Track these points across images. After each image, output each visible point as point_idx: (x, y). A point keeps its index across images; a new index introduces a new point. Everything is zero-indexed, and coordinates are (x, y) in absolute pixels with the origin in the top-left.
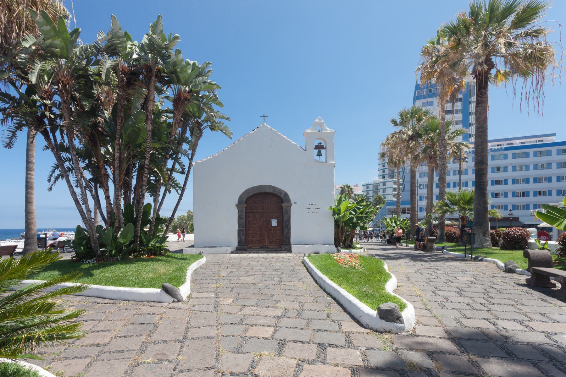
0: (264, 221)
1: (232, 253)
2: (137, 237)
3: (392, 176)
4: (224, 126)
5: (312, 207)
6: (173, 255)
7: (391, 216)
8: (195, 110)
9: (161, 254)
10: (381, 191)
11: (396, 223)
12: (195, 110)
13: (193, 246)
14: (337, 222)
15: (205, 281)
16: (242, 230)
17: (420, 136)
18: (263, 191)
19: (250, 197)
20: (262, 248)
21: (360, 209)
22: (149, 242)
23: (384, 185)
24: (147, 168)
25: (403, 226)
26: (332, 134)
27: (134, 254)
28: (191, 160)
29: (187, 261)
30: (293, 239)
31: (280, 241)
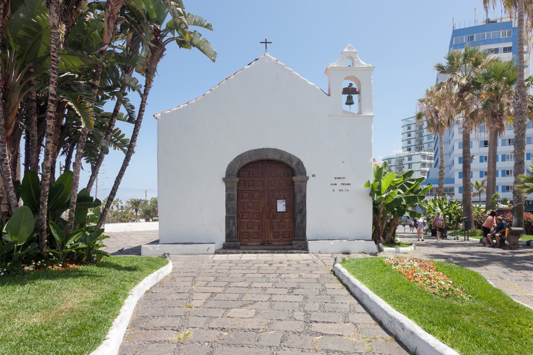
0: (265, 202)
1: (217, 252)
2: (42, 231)
3: (419, 148)
4: (201, 39)
5: (339, 182)
6: (114, 260)
7: (433, 197)
8: (152, 7)
9: (90, 261)
10: (406, 167)
11: (440, 206)
12: (152, 7)
13: (157, 242)
14: (375, 205)
15: (159, 322)
16: (233, 218)
17: (478, 86)
18: (265, 158)
19: (244, 167)
20: (263, 244)
21: (411, 185)
22: (67, 240)
23: (410, 159)
24: (52, 101)
25: (451, 211)
26: (369, 70)
27: (36, 262)
28: (144, 96)
29: (136, 273)
30: (309, 233)
31: (290, 235)
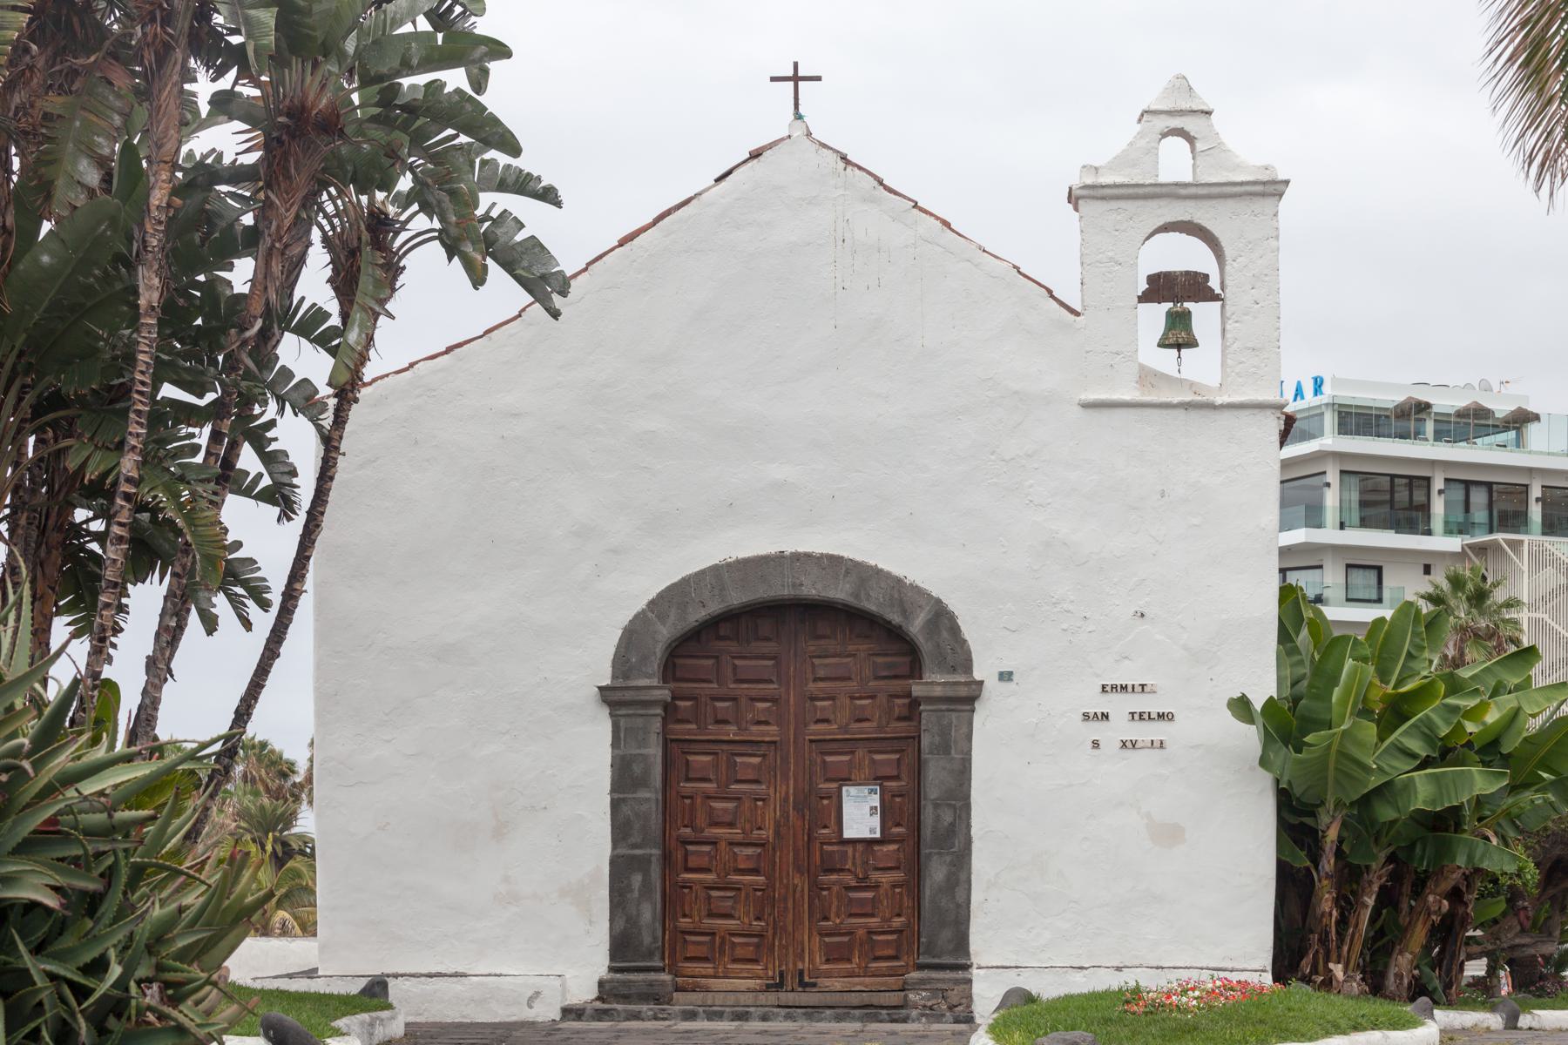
5: (1119, 706)
16: (641, 864)
